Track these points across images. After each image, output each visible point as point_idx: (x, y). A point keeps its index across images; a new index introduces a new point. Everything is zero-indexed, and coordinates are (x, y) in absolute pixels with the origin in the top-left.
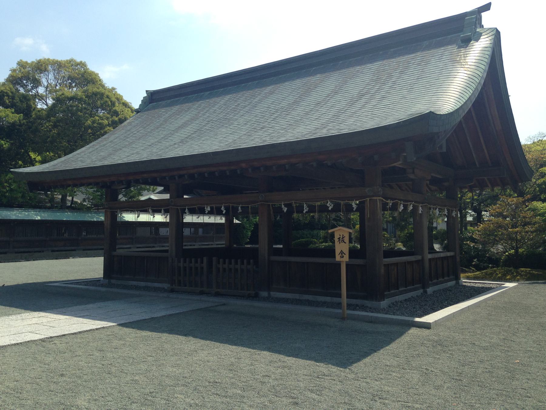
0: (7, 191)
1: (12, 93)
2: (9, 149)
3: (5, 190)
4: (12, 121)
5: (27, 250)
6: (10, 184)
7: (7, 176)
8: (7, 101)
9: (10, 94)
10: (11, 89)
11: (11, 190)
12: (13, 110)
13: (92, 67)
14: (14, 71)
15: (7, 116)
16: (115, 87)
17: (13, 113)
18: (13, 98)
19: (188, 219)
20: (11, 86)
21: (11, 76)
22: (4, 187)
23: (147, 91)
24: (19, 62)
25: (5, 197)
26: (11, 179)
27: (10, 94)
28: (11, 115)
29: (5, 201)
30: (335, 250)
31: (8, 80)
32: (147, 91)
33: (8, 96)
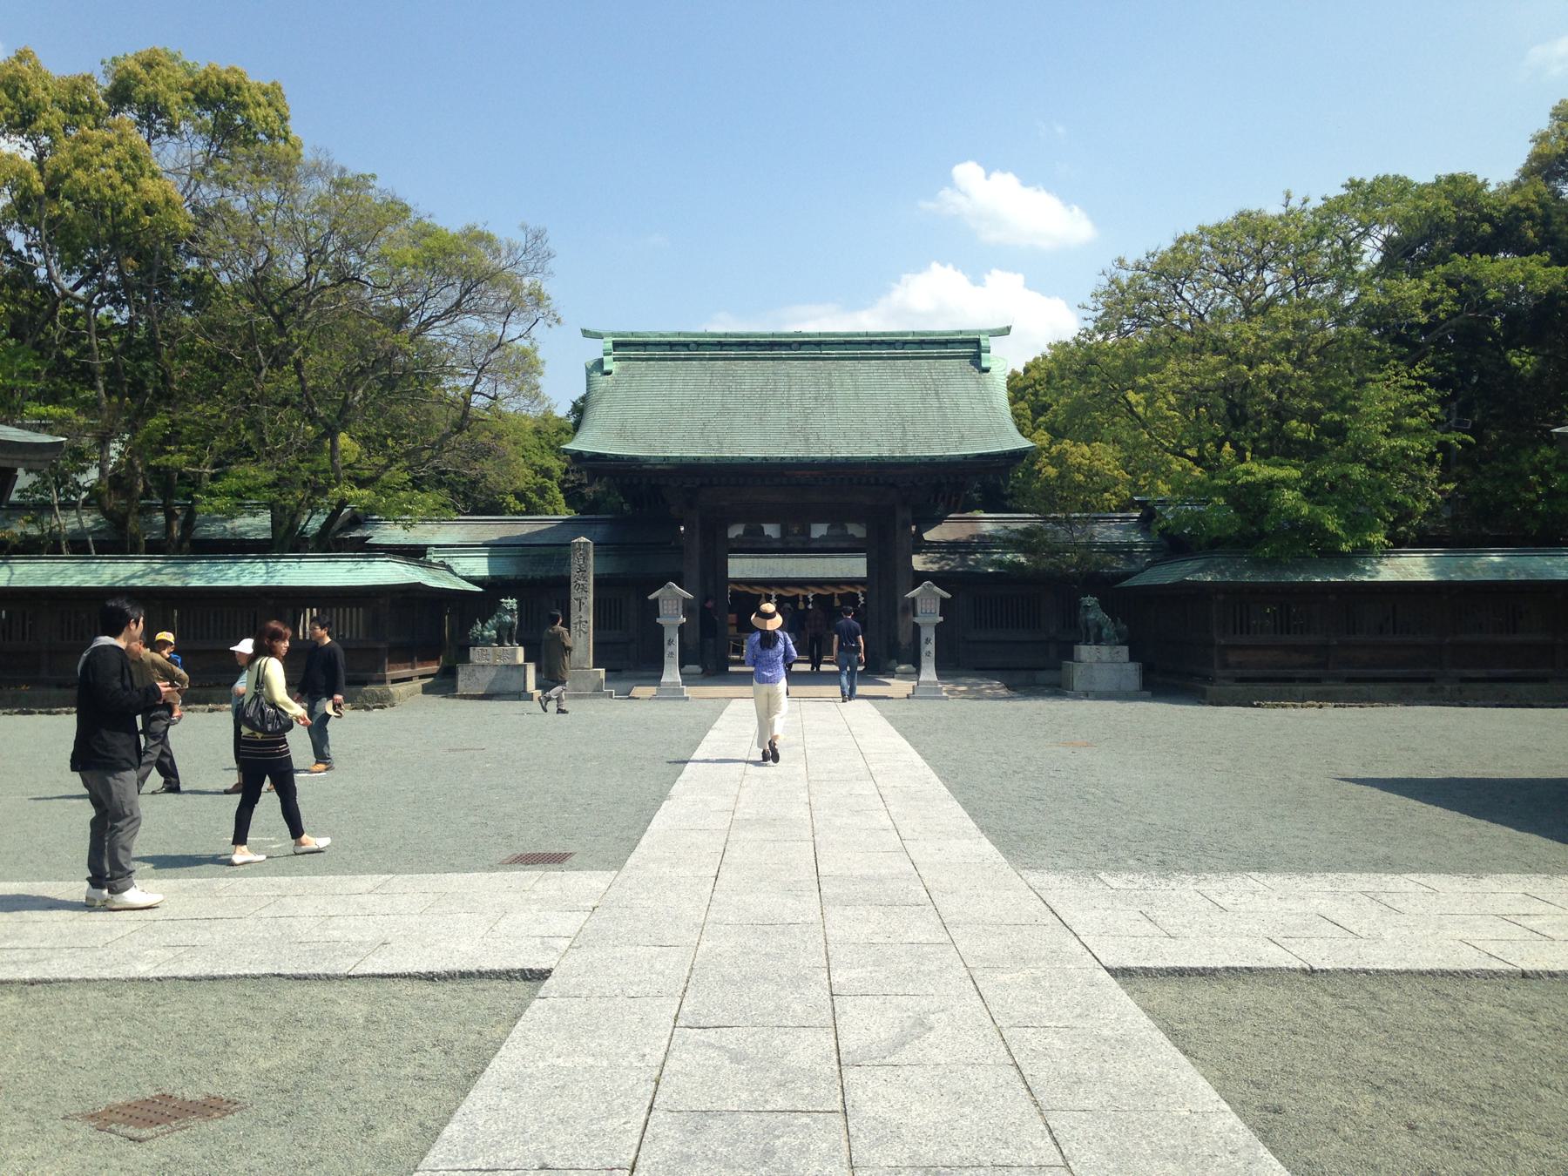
0: (1539, 497)
1: (1542, 206)
2: (1539, 375)
3: (1532, 496)
4: (1543, 290)
5: (1482, 673)
6: (1546, 478)
7: (1536, 451)
8: (1531, 234)
9: (1538, 211)
10: (1538, 194)
11: (1552, 495)
12: (1547, 257)
13: (400, 195)
14: (1542, 138)
15: (1530, 277)
16: (471, 223)
17: (1547, 265)
18: (1546, 221)
19: (856, 566)
20: (1541, 187)
21: (1535, 157)
22: (1529, 487)
23: (987, 177)
24: (1556, 108)
25: (1536, 515)
26: (1548, 461)
27: (1538, 211)
28: (1541, 272)
29: (1534, 527)
30: (1059, 689)
31: (1528, 172)
32: (987, 177)
33: (1531, 217)
